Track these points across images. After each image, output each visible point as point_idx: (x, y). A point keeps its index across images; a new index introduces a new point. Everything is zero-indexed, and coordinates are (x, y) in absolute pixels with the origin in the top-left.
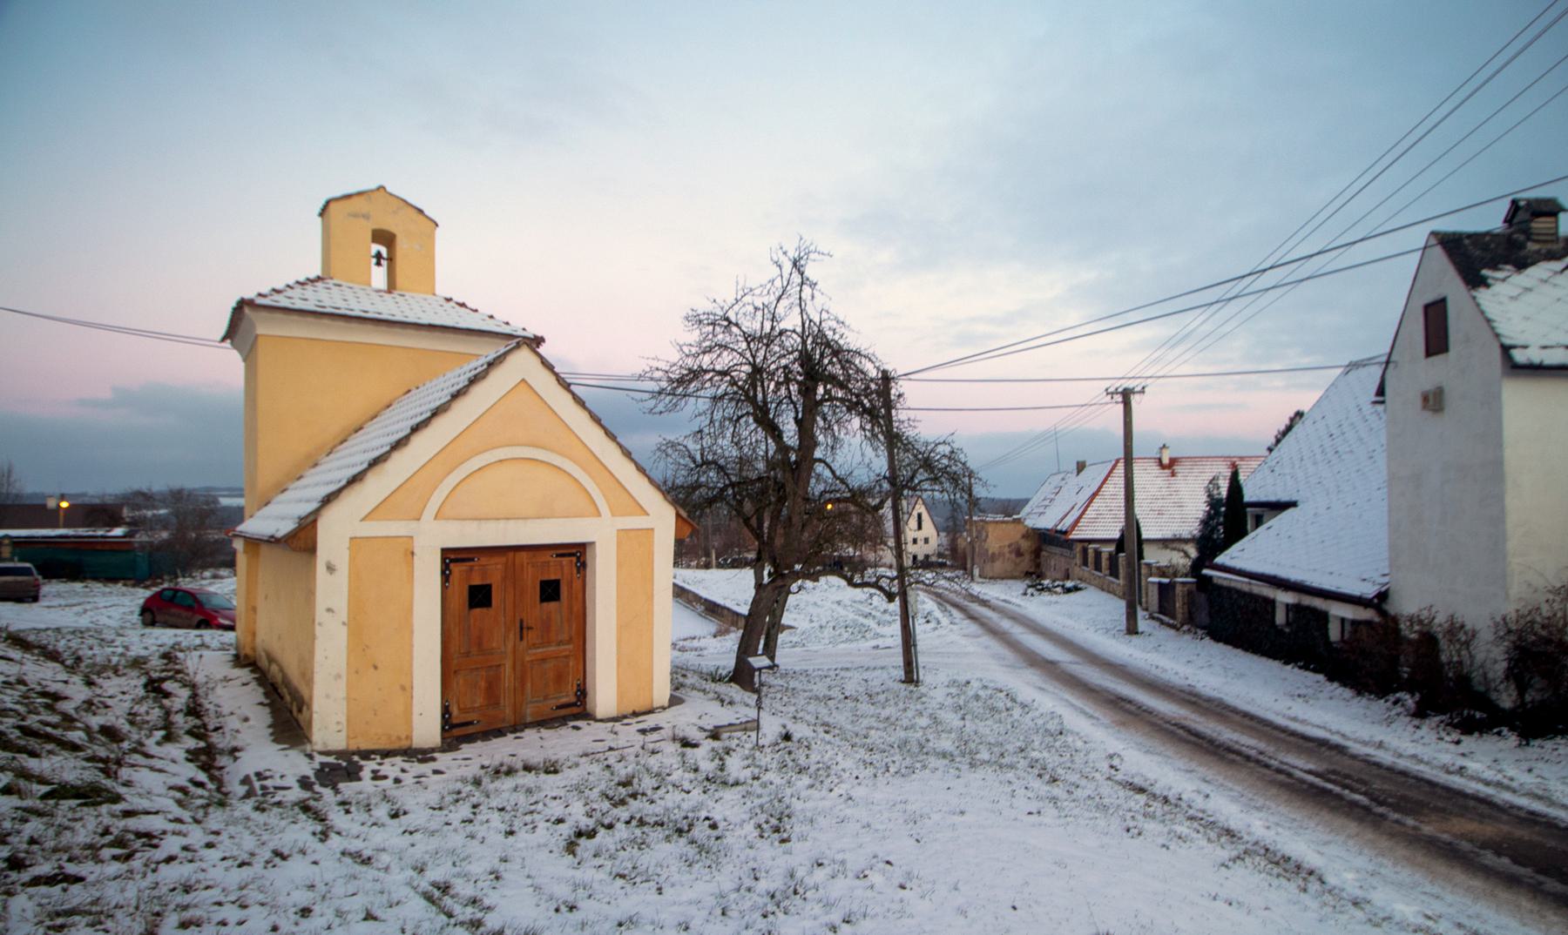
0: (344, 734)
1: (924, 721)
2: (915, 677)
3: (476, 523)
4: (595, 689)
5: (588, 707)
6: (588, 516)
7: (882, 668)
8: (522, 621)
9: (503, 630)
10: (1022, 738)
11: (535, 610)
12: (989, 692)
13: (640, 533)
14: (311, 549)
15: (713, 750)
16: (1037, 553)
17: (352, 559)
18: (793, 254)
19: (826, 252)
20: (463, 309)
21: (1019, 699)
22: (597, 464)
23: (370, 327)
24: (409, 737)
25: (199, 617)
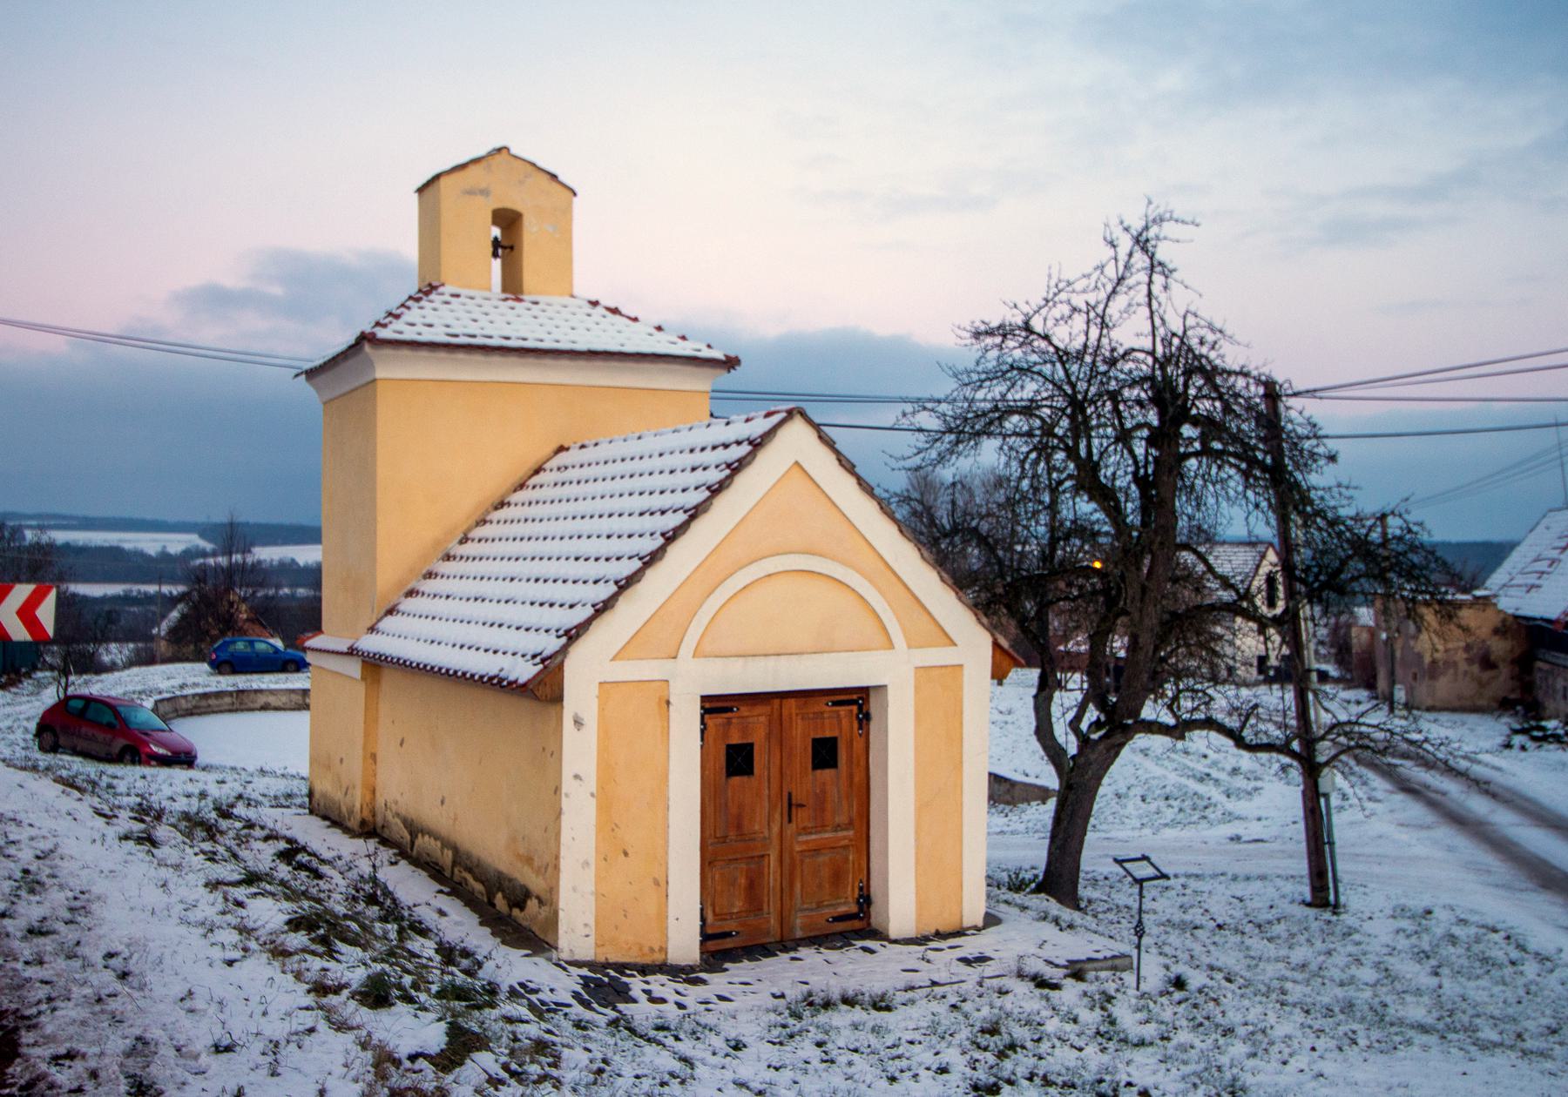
0: (592, 940)
1: (1367, 974)
2: (1332, 898)
3: (741, 660)
4: (886, 895)
5: (873, 921)
6: (876, 649)
7: (1263, 878)
8: (790, 795)
9: (766, 804)
10: (1548, 1012)
11: (807, 782)
12: (1473, 930)
13: (943, 670)
14: (557, 699)
15: (1085, 994)
16: (1523, 665)
17: (602, 709)
18: (1137, 225)
19: (1188, 219)
20: (617, 317)
21: (1532, 946)
22: (889, 574)
23: (513, 359)
24: (664, 950)
25: (120, 743)
